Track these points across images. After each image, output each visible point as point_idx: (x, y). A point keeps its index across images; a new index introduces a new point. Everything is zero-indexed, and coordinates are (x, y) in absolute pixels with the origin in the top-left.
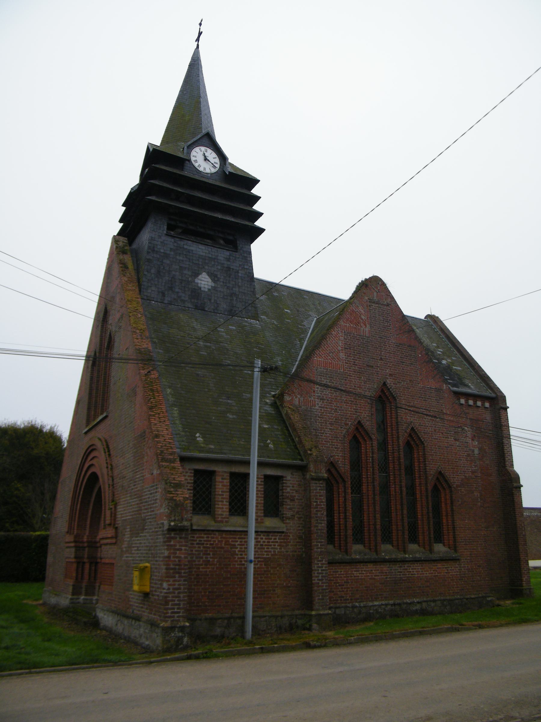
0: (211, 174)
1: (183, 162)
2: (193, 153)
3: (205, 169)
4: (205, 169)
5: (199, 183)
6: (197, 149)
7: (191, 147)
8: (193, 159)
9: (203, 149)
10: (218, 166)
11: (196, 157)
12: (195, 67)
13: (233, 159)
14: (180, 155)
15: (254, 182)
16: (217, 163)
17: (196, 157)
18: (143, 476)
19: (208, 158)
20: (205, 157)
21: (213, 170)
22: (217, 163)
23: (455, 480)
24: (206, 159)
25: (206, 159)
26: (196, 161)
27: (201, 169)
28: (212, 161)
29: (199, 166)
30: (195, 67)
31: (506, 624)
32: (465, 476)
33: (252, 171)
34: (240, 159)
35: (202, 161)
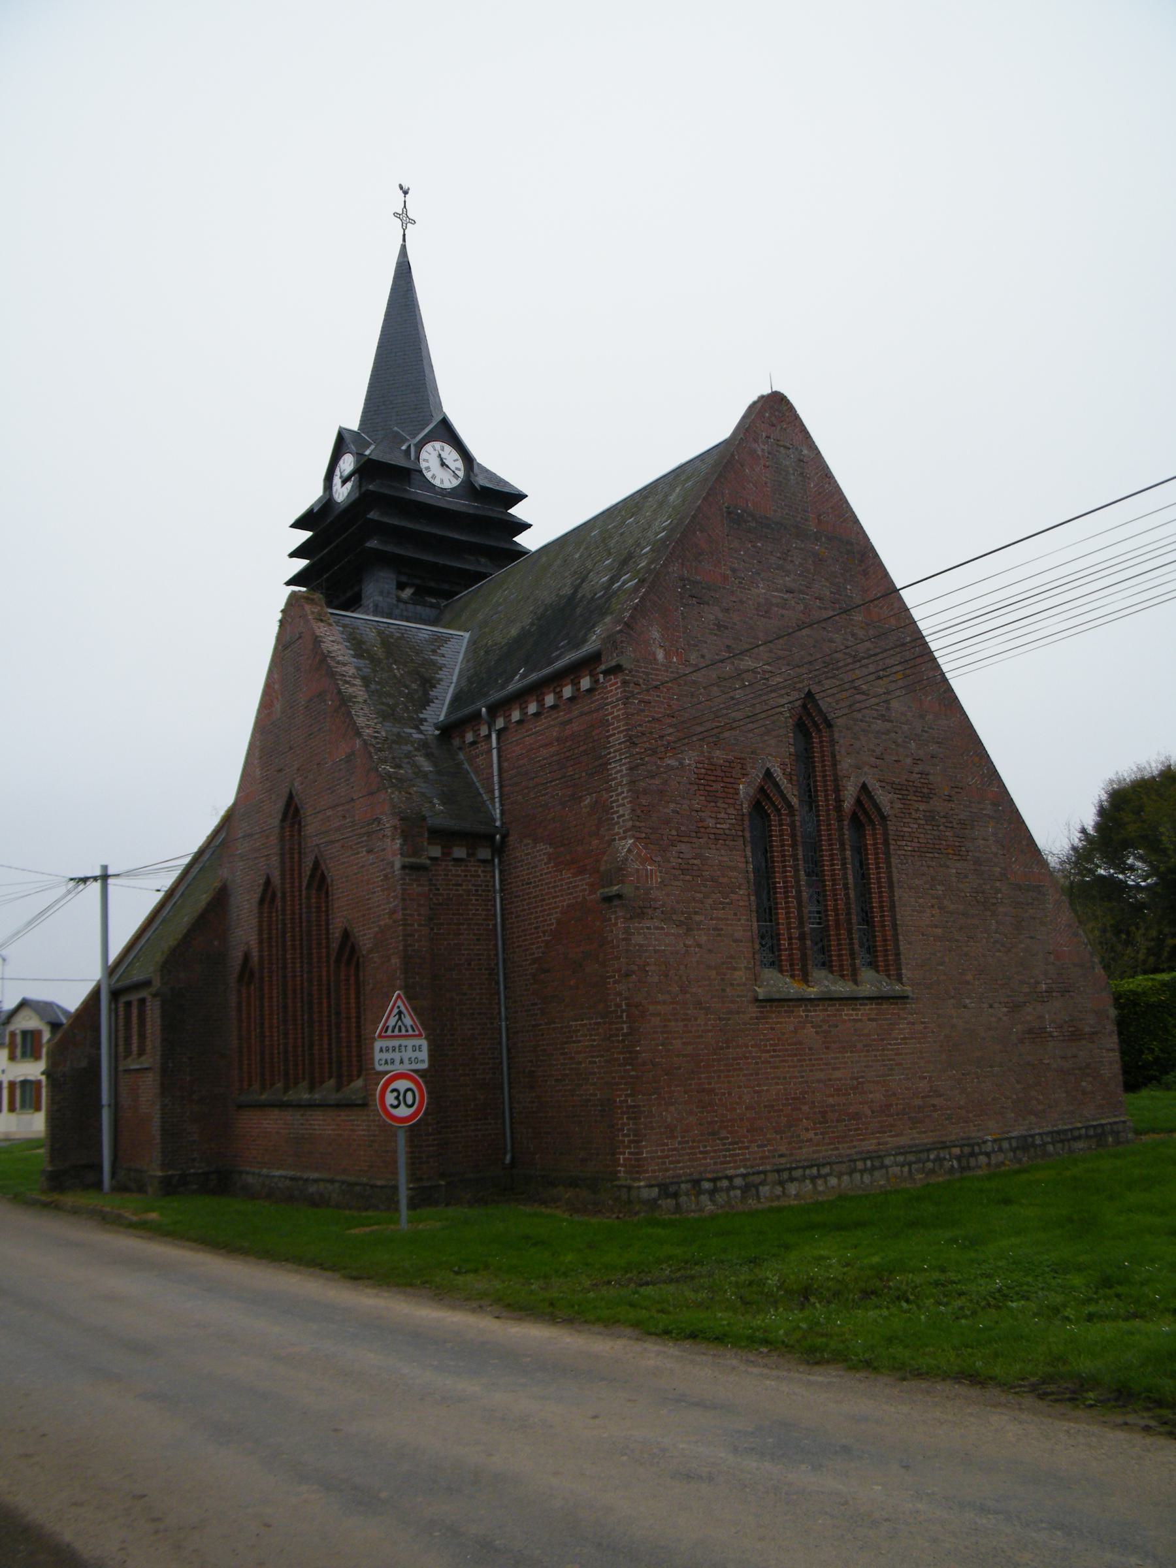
0: (453, 489)
1: (410, 474)
2: (424, 455)
3: (442, 481)
4: (442, 481)
5: (434, 512)
6: (428, 447)
7: (420, 446)
8: (423, 465)
9: (438, 445)
10: (461, 474)
11: (427, 461)
12: (403, 272)
13: (481, 457)
14: (403, 463)
15: (519, 497)
16: (459, 469)
17: (427, 461)
18: (638, 1154)
19: (447, 462)
20: (441, 460)
21: (456, 483)
22: (459, 469)
23: (365, 939)
24: (443, 464)
25: (443, 464)
26: (428, 468)
27: (437, 482)
28: (453, 466)
29: (434, 477)
30: (403, 272)
31: (751, 1340)
32: (380, 926)
33: (515, 478)
34: (498, 459)
35: (438, 469)
